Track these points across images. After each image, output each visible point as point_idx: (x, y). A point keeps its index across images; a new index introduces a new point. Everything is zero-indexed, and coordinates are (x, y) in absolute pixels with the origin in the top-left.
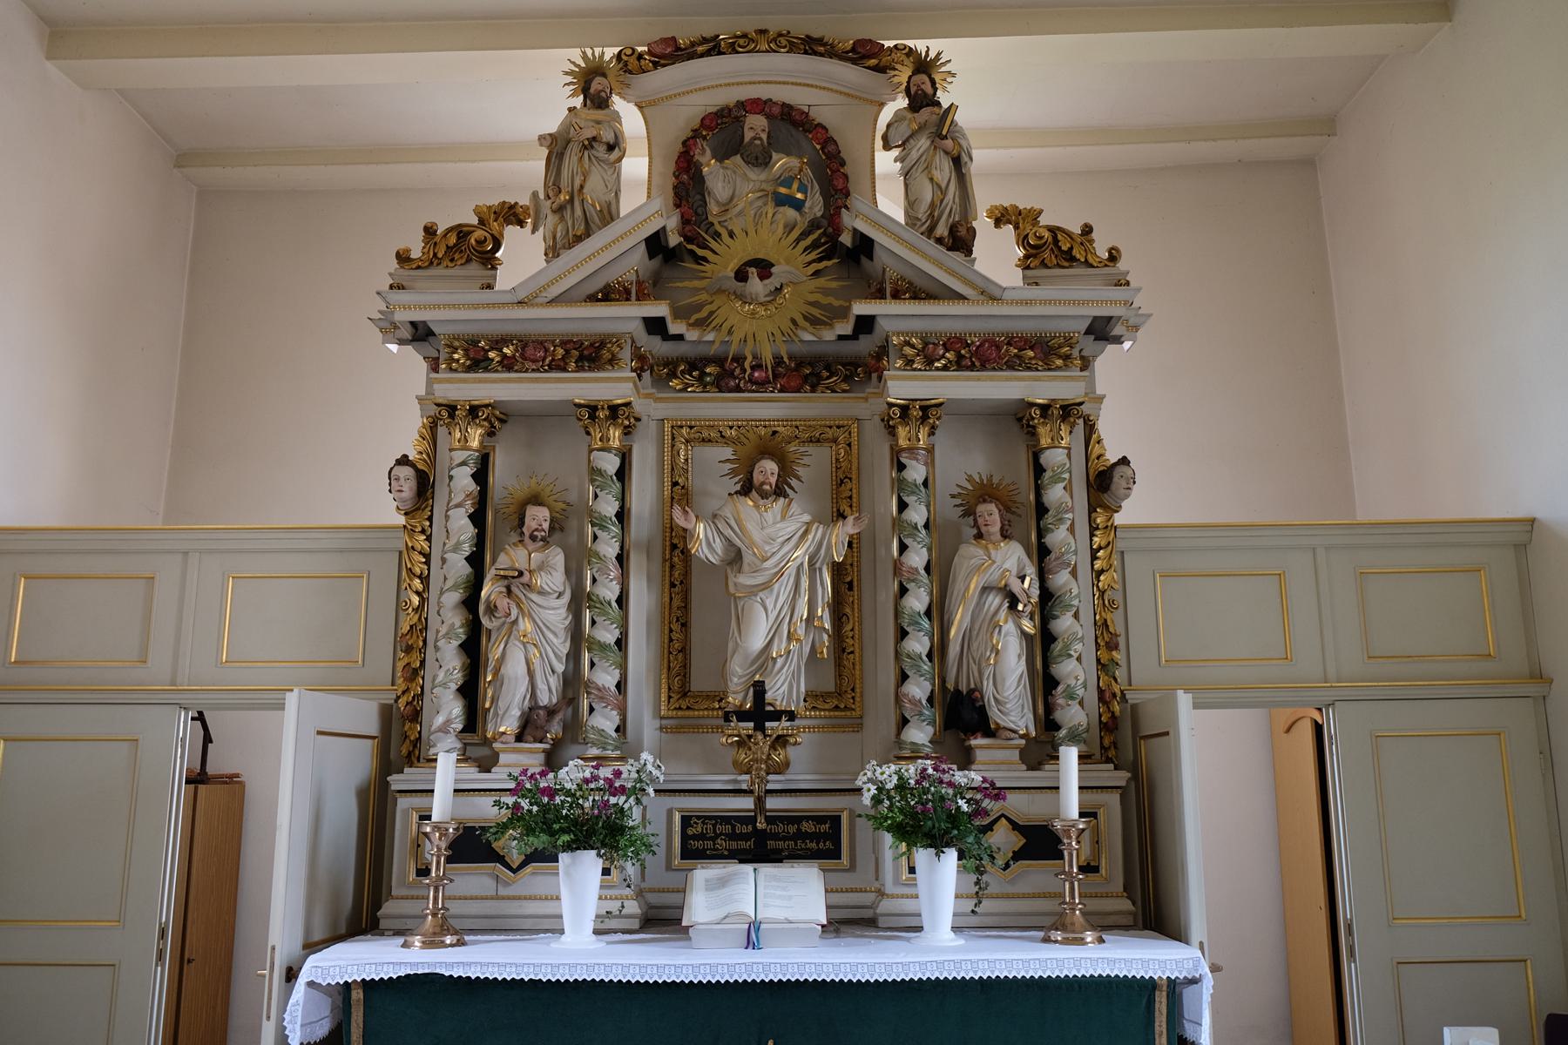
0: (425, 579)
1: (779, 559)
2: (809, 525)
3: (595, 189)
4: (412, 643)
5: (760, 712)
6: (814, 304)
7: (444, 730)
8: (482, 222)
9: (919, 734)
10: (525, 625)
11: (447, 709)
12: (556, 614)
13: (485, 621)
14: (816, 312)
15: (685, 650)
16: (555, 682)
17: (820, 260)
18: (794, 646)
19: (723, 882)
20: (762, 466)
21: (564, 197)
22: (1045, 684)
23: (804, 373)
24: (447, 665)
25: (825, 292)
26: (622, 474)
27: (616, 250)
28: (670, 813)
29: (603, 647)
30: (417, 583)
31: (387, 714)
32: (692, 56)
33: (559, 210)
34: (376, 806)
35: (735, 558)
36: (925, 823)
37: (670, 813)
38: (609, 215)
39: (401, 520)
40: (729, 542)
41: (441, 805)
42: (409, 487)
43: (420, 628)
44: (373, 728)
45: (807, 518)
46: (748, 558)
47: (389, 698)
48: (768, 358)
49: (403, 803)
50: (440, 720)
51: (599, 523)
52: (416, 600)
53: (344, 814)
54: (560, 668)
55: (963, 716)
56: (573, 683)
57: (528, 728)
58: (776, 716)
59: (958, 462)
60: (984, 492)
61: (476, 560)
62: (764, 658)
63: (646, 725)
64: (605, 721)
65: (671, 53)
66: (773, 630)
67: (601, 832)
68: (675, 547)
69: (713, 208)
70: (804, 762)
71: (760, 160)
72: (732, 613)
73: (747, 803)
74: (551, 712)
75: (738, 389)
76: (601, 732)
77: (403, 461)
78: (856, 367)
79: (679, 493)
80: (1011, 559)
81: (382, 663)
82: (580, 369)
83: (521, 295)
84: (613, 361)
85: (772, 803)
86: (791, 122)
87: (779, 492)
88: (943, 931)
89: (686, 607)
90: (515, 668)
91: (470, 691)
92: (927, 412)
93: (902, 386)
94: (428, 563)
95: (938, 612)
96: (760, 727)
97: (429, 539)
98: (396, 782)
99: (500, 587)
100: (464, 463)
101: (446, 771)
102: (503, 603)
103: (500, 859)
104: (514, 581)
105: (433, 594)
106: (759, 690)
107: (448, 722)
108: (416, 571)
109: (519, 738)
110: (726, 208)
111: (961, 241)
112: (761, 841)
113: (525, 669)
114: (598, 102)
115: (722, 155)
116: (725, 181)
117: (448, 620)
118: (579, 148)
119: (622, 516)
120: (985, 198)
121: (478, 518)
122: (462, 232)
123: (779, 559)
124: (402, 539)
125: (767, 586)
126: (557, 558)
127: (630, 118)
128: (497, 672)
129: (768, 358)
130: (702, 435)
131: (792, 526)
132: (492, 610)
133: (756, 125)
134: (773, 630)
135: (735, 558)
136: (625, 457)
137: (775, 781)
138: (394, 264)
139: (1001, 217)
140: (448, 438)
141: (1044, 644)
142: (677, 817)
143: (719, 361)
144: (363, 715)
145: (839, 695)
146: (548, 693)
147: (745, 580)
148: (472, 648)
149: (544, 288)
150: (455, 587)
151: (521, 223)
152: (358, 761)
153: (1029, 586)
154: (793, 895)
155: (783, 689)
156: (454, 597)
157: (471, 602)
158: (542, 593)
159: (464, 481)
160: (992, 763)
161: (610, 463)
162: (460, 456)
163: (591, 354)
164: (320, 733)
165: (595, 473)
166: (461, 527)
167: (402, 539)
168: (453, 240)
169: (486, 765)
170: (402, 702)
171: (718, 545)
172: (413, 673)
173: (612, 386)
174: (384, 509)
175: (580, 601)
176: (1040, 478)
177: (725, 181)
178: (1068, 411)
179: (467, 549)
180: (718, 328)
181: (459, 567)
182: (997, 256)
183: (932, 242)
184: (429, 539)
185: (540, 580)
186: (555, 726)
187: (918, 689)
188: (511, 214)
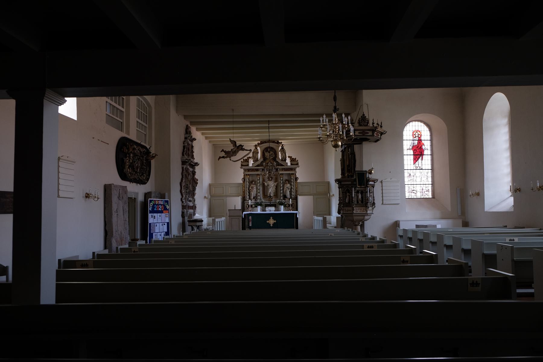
1: (271, 186)
4: (244, 192)
5: (270, 197)
9: (282, 198)
12: (255, 190)
22: (291, 194)
36: (281, 204)
55: (285, 197)
57: (254, 198)
59: (285, 178)
60: (286, 180)
63: (262, 198)
65: (262, 143)
66: (271, 191)
67: (260, 205)
68: (263, 184)
70: (273, 200)
72: (268, 189)
79: (264, 180)
80: (289, 185)
86: (272, 149)
88: (282, 210)
92: (282, 174)
93: (281, 172)
95: (283, 189)
104: (252, 187)
111: (285, 160)
112: (271, 205)
113: (253, 194)
114: (256, 148)
116: (267, 154)
120: (287, 156)
123: (271, 186)
127: (258, 148)
134: (271, 191)
138: (334, 149)
139: (289, 157)
141: (291, 192)
145: (276, 195)
148: (249, 193)
153: (290, 187)
154: (273, 209)
155: (272, 195)
160: (287, 200)
163: (257, 170)
176: (291, 179)
177: (267, 154)
178: (293, 174)
182: (288, 161)
183: (196, 203)
186: (255, 198)
187: (282, 195)
188: (250, 158)
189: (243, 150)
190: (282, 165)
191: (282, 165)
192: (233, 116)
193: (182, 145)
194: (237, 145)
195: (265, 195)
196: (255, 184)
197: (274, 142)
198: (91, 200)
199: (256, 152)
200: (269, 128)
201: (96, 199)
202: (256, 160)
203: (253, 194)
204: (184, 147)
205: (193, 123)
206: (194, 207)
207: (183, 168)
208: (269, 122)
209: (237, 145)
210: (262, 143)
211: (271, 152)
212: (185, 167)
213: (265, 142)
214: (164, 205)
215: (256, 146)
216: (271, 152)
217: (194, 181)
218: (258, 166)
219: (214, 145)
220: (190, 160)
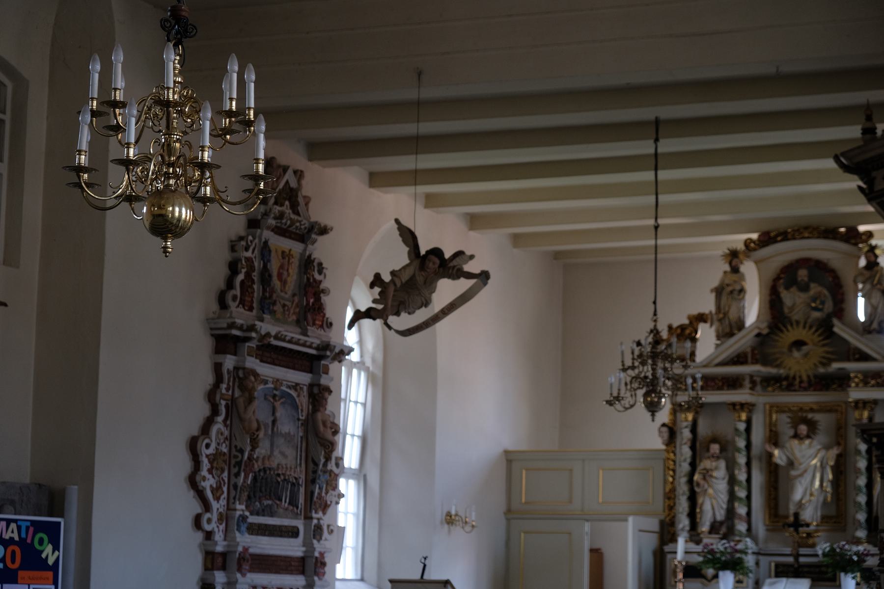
0: (674, 471)
2: (819, 450)
3: (733, 315)
4: (670, 496)
5: (797, 524)
6: (823, 357)
7: (683, 529)
8: (691, 323)
10: (710, 491)
11: (684, 522)
13: (696, 489)
14: (824, 361)
15: (776, 499)
16: (723, 512)
17: (823, 340)
18: (812, 498)
19: (774, 583)
20: (804, 424)
21: (721, 316)
23: (823, 383)
24: (683, 505)
25: (828, 352)
26: (748, 430)
27: (741, 342)
28: (770, 563)
29: (740, 499)
30: (671, 473)
31: (662, 523)
32: (776, 242)
33: (720, 320)
34: (660, 557)
35: (791, 464)
37: (770, 563)
38: (740, 325)
39: (664, 447)
40: (788, 458)
41: (680, 556)
42: (666, 435)
43: (673, 490)
44: (656, 528)
45: (819, 447)
46: (796, 464)
47: (662, 517)
48: (805, 378)
49: (669, 556)
50: (681, 526)
51: (739, 450)
52: (671, 479)
53: (649, 559)
54: (725, 506)
56: (731, 512)
58: (802, 526)
61: (693, 465)
62: (800, 505)
64: (742, 527)
65: (767, 239)
67: (734, 564)
69: (786, 310)
71: (805, 288)
73: (791, 560)
74: (721, 523)
75: (795, 391)
76: (740, 531)
77: (664, 425)
78: (842, 381)
81: (659, 504)
82: (728, 389)
83: (704, 363)
84: (741, 386)
85: (802, 560)
87: (808, 437)
89: (776, 481)
90: (707, 507)
91: (692, 515)
93: (855, 394)
94: (675, 464)
96: (797, 531)
97: (675, 455)
98: (667, 549)
99: (701, 476)
100: (686, 427)
101: (681, 544)
102: (702, 482)
103: (703, 577)
104: (707, 474)
105: (677, 477)
106: (796, 515)
107: (684, 527)
108: (670, 467)
109: (710, 532)
110: (792, 308)
113: (713, 506)
114: (735, 270)
115: (787, 288)
116: (789, 298)
117: (683, 488)
118: (729, 292)
119: (748, 447)
121: (693, 448)
122: (682, 328)
124: (665, 455)
125: (801, 475)
126: (722, 464)
128: (701, 508)
129: (805, 378)
130: (780, 409)
131: (812, 451)
132: (698, 485)
133: (803, 274)
135: (791, 464)
136: (749, 422)
137: (803, 551)
140: (681, 416)
142: (773, 565)
143: (787, 378)
144: (653, 524)
145: (836, 516)
146: (720, 515)
147: (793, 473)
148: (693, 499)
149: (713, 360)
150: (685, 476)
151: (705, 322)
152: (652, 541)
155: (809, 514)
156: (684, 480)
157: (690, 481)
158: (716, 478)
159: (687, 434)
161: (742, 426)
162: (685, 424)
163: (733, 383)
164: (641, 531)
165: (737, 430)
166: (686, 451)
167: (665, 455)
168: (679, 331)
169: (698, 543)
170: (668, 519)
171: (784, 458)
172: (671, 508)
173: (741, 396)
174: (658, 443)
175: (732, 481)
177: (789, 298)
179: (689, 460)
180: (784, 368)
181: (686, 467)
184: (675, 455)
185: (715, 474)
186: (724, 527)
188: (701, 318)
189: (458, 274)
190: (865, 357)
191: (865, 357)
192: (418, 108)
193: (226, 256)
194: (423, 252)
195: (782, 518)
196: (726, 449)
197: (830, 233)
198: (457, 530)
199: (729, 292)
200: (656, 162)
201: (468, 528)
202: (729, 327)
203: (713, 506)
204: (233, 267)
205: (323, 151)
206: (310, 564)
207: (218, 368)
208: (657, 129)
209: (423, 252)
210: (767, 239)
211: (815, 289)
212: (229, 362)
213: (785, 236)
214: (22, 543)
215: (733, 256)
216: (815, 289)
217: (317, 434)
218: (739, 359)
219: (557, 255)
220: (252, 328)
